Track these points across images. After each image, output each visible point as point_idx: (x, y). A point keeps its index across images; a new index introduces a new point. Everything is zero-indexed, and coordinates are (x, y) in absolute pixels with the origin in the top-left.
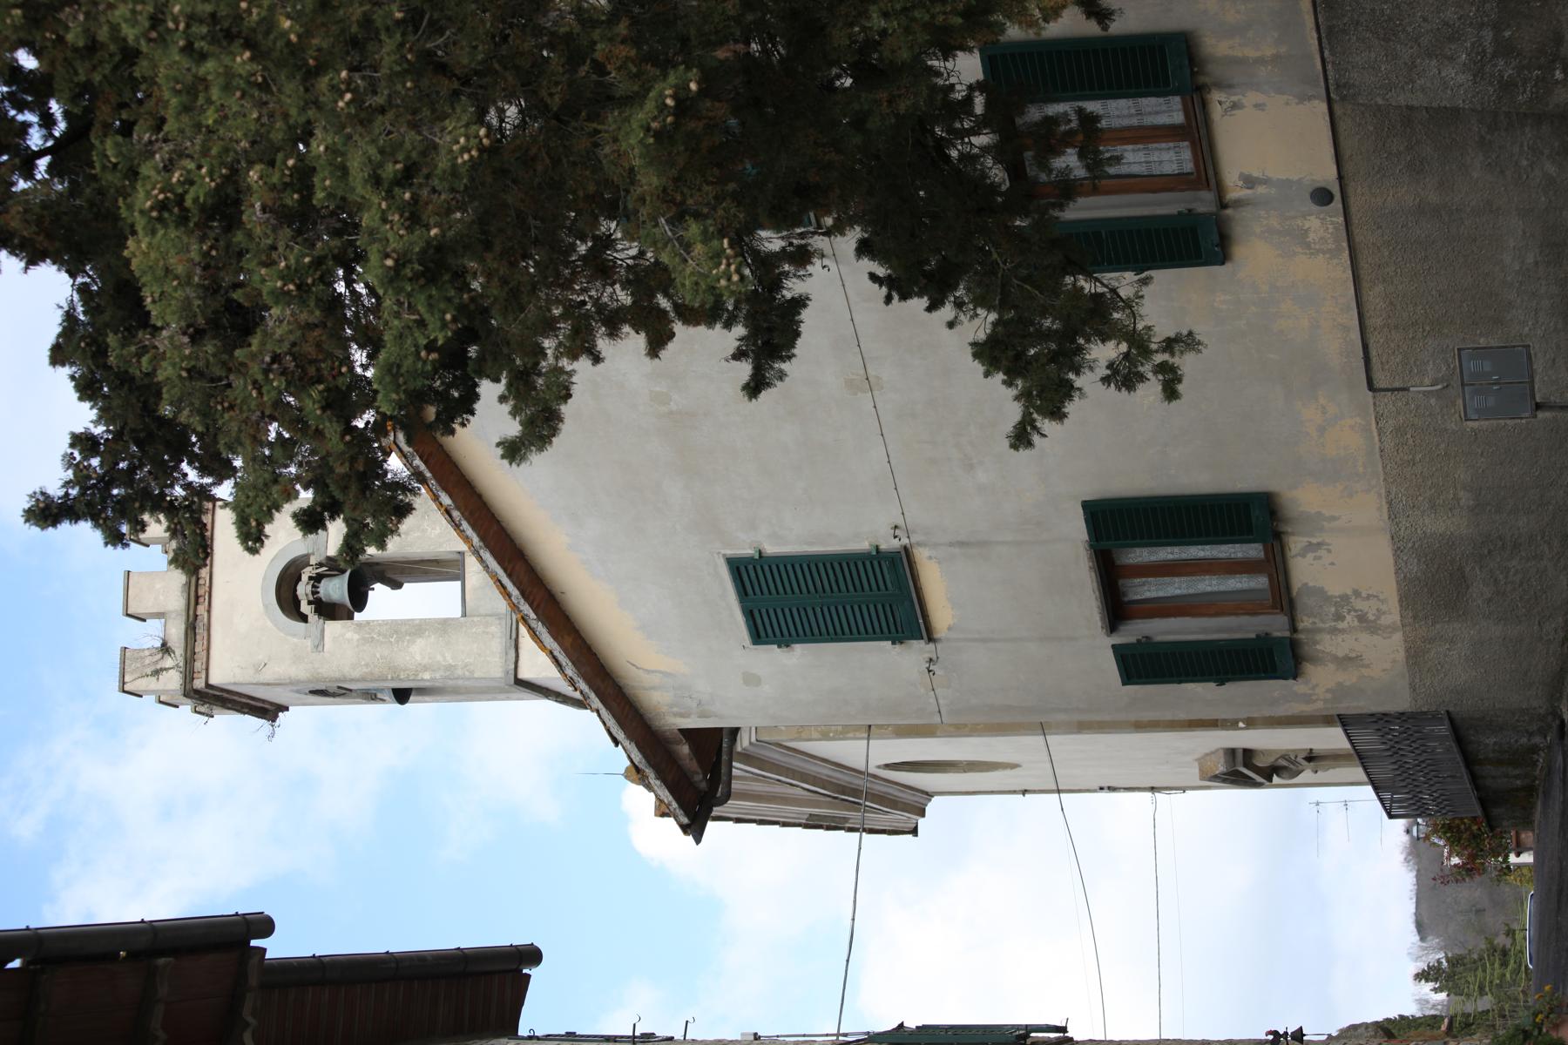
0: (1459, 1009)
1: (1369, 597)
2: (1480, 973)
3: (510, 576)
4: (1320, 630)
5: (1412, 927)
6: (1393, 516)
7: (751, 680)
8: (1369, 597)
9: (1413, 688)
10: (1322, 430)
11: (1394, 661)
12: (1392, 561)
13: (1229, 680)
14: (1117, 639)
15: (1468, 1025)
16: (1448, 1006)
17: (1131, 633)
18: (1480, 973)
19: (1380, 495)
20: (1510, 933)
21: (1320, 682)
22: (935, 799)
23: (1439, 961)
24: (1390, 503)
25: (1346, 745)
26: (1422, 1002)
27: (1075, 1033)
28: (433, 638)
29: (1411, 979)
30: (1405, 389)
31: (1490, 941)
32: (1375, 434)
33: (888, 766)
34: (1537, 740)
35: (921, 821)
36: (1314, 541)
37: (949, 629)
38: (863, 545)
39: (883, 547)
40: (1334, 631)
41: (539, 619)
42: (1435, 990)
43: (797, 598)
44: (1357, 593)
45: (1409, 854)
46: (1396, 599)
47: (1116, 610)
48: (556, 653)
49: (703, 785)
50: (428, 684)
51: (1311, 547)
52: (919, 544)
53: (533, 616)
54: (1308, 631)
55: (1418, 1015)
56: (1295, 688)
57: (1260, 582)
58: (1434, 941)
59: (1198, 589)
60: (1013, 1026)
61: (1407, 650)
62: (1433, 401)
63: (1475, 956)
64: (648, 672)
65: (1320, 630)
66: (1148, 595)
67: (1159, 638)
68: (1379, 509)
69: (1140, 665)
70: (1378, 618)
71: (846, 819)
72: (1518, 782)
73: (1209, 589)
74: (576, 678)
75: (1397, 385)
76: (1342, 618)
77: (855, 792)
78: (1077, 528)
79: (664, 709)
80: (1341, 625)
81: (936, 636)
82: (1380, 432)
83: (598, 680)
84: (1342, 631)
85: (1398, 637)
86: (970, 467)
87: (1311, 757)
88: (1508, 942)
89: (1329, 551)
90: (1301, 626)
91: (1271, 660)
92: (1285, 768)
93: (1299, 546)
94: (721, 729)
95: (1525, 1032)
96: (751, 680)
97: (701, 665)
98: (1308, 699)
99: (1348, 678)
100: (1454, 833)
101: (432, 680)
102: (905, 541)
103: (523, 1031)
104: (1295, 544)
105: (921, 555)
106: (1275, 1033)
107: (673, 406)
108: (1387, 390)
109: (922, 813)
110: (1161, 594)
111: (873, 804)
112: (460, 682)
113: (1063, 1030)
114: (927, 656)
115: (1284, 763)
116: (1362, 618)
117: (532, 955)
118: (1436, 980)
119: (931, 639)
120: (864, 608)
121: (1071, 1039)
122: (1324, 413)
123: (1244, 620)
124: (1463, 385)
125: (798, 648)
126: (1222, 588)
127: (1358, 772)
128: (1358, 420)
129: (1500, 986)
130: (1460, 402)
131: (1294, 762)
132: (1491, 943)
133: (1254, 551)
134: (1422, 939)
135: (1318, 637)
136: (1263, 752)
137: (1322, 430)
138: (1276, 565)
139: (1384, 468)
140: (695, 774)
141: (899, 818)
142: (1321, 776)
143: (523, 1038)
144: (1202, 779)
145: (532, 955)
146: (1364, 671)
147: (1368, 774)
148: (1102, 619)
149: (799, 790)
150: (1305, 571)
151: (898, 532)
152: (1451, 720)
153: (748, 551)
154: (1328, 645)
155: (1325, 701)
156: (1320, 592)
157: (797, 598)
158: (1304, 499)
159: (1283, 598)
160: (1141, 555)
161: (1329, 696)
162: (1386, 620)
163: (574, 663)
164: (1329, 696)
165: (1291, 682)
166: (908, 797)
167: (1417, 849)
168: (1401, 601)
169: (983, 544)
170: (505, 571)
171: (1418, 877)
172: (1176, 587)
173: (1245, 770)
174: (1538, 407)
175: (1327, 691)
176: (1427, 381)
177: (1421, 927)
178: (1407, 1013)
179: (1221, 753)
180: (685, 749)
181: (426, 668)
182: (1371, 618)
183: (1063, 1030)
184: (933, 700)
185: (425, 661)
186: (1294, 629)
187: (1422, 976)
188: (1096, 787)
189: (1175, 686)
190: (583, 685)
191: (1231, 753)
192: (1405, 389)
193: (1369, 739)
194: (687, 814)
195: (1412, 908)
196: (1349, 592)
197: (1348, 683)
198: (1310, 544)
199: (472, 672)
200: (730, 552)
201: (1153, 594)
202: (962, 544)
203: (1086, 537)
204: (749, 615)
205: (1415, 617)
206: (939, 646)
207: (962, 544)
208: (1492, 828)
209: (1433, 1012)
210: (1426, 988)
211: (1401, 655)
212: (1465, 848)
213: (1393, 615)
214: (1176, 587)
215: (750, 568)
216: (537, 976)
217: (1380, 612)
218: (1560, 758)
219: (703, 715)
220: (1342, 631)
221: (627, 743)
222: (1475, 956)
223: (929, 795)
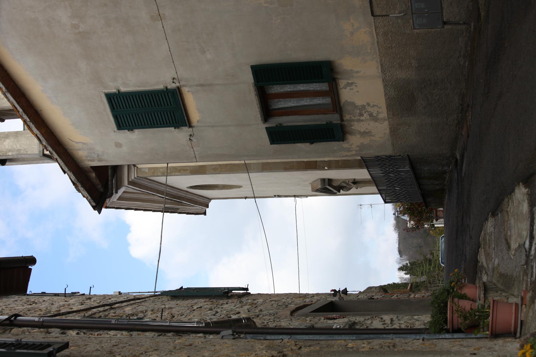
0: (414, 280)
1: (373, 106)
2: (421, 268)
3: (18, 104)
4: (353, 120)
5: (397, 252)
6: (383, 71)
7: (118, 145)
8: (373, 106)
9: (393, 145)
10: (352, 33)
11: (385, 134)
12: (383, 90)
13: (315, 142)
14: (268, 125)
15: (418, 286)
16: (410, 280)
17: (274, 122)
18: (421, 268)
19: (377, 62)
20: (432, 254)
21: (354, 141)
22: (212, 201)
23: (407, 264)
24: (382, 65)
25: (369, 177)
26: (401, 278)
27: (252, 291)
28: (12, 139)
29: (397, 270)
30: (388, 16)
31: (425, 257)
32: (375, 35)
33: (191, 187)
34: (446, 168)
35: (207, 209)
36: (350, 82)
37: (198, 122)
38: (161, 87)
39: (169, 87)
40: (359, 121)
41: (31, 121)
42: (406, 274)
43: (136, 110)
44: (368, 104)
45: (396, 227)
46: (385, 107)
47: (267, 113)
48: (38, 135)
49: (102, 190)
50: (11, 157)
51: (349, 85)
52: (184, 86)
53: (28, 120)
54: (348, 121)
55: (400, 282)
56: (343, 145)
57: (327, 100)
58: (405, 257)
59: (300, 101)
60: (225, 288)
61: (390, 129)
62: (400, 21)
63: (420, 262)
64: (77, 143)
65: (353, 120)
66: (280, 106)
67: (285, 124)
68: (377, 68)
69: (278, 136)
70: (378, 115)
71: (178, 209)
72: (438, 187)
73: (306, 104)
74: (47, 145)
75: (384, 14)
76: (362, 115)
77: (179, 198)
78: (249, 77)
79: (84, 158)
80: (362, 118)
81: (193, 125)
82: (377, 34)
83: (56, 147)
84: (363, 121)
85: (386, 123)
86: (204, 52)
87: (355, 182)
88: (431, 257)
89: (356, 86)
90: (345, 118)
91: (334, 133)
92: (345, 187)
93: (344, 84)
94: (108, 166)
95: (448, 291)
96: (118, 145)
97: (98, 140)
98: (349, 150)
99: (366, 141)
100: (411, 211)
101: (12, 155)
102: (178, 84)
103: (28, 293)
104: (342, 83)
105: (185, 90)
106: (335, 291)
107: (81, 30)
108: (379, 16)
109: (208, 207)
110: (286, 106)
111: (189, 203)
112: (23, 156)
113: (247, 289)
114: (189, 133)
115: (345, 185)
116: (371, 115)
117: (32, 260)
118: (406, 270)
119: (190, 126)
120: (162, 113)
121: (250, 293)
122: (353, 26)
123: (321, 116)
124: (412, 14)
125: (136, 131)
126: (311, 103)
127: (374, 189)
128: (367, 29)
129: (429, 272)
130: (411, 21)
131: (348, 184)
132: (425, 257)
133: (323, 87)
134: (401, 257)
135: (352, 123)
136: (336, 180)
137: (352, 33)
138: (334, 93)
139: (379, 50)
140: (99, 185)
141: (199, 208)
142: (360, 190)
143: (28, 295)
144: (313, 191)
145: (32, 260)
146: (373, 138)
147: (379, 190)
148: (261, 117)
149: (157, 197)
150: (346, 95)
151: (174, 81)
152: (410, 159)
153: (114, 91)
154: (358, 127)
155: (356, 151)
156: (353, 104)
157: (136, 110)
158: (346, 63)
159: (337, 106)
160: (277, 89)
161: (358, 149)
162: (381, 116)
163: (46, 139)
164: (358, 149)
165: (341, 143)
166: (201, 200)
167: (399, 225)
168: (387, 108)
169: (210, 85)
170: (16, 101)
171: (399, 235)
172: (291, 103)
173: (329, 188)
174: (445, 23)
175: (357, 146)
176: (397, 12)
177: (400, 252)
178: (396, 282)
179: (319, 181)
180: (94, 175)
181: (10, 151)
182: (375, 115)
183: (247, 289)
184: (192, 152)
185: (10, 148)
186: (342, 120)
187: (401, 269)
188: (273, 195)
189: (293, 145)
190: (50, 149)
191: (323, 180)
192: (388, 16)
193: (377, 172)
194: (95, 202)
195: (397, 246)
196: (365, 104)
197: (365, 143)
198: (348, 83)
199: (27, 152)
200: (106, 91)
201: (283, 106)
202: (201, 85)
203: (253, 81)
204: (116, 117)
205: (393, 115)
206: (194, 129)
207: (201, 85)
208: (427, 207)
209: (405, 282)
210: (402, 274)
211: (388, 131)
212: (416, 217)
213: (384, 114)
214: (291, 103)
215: (115, 97)
216: (35, 269)
217: (378, 113)
218: (456, 175)
219: (100, 160)
220: (363, 121)
221: (69, 172)
222: (420, 262)
223: (210, 199)
